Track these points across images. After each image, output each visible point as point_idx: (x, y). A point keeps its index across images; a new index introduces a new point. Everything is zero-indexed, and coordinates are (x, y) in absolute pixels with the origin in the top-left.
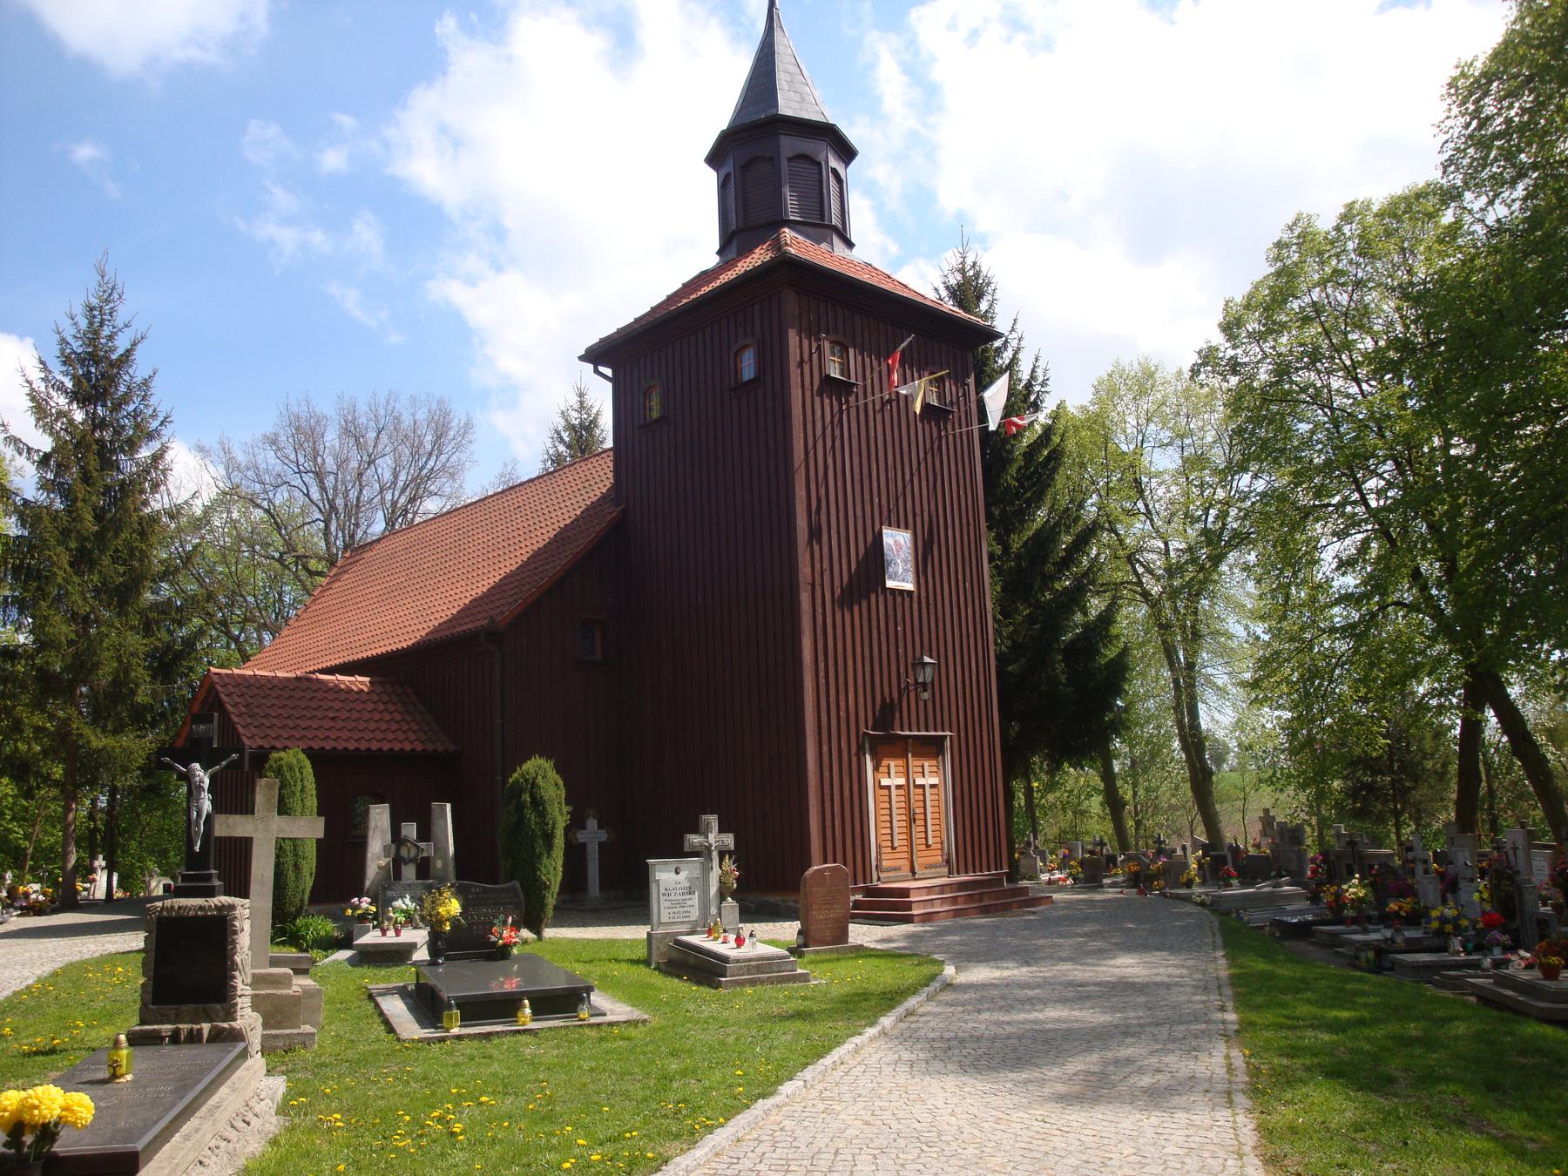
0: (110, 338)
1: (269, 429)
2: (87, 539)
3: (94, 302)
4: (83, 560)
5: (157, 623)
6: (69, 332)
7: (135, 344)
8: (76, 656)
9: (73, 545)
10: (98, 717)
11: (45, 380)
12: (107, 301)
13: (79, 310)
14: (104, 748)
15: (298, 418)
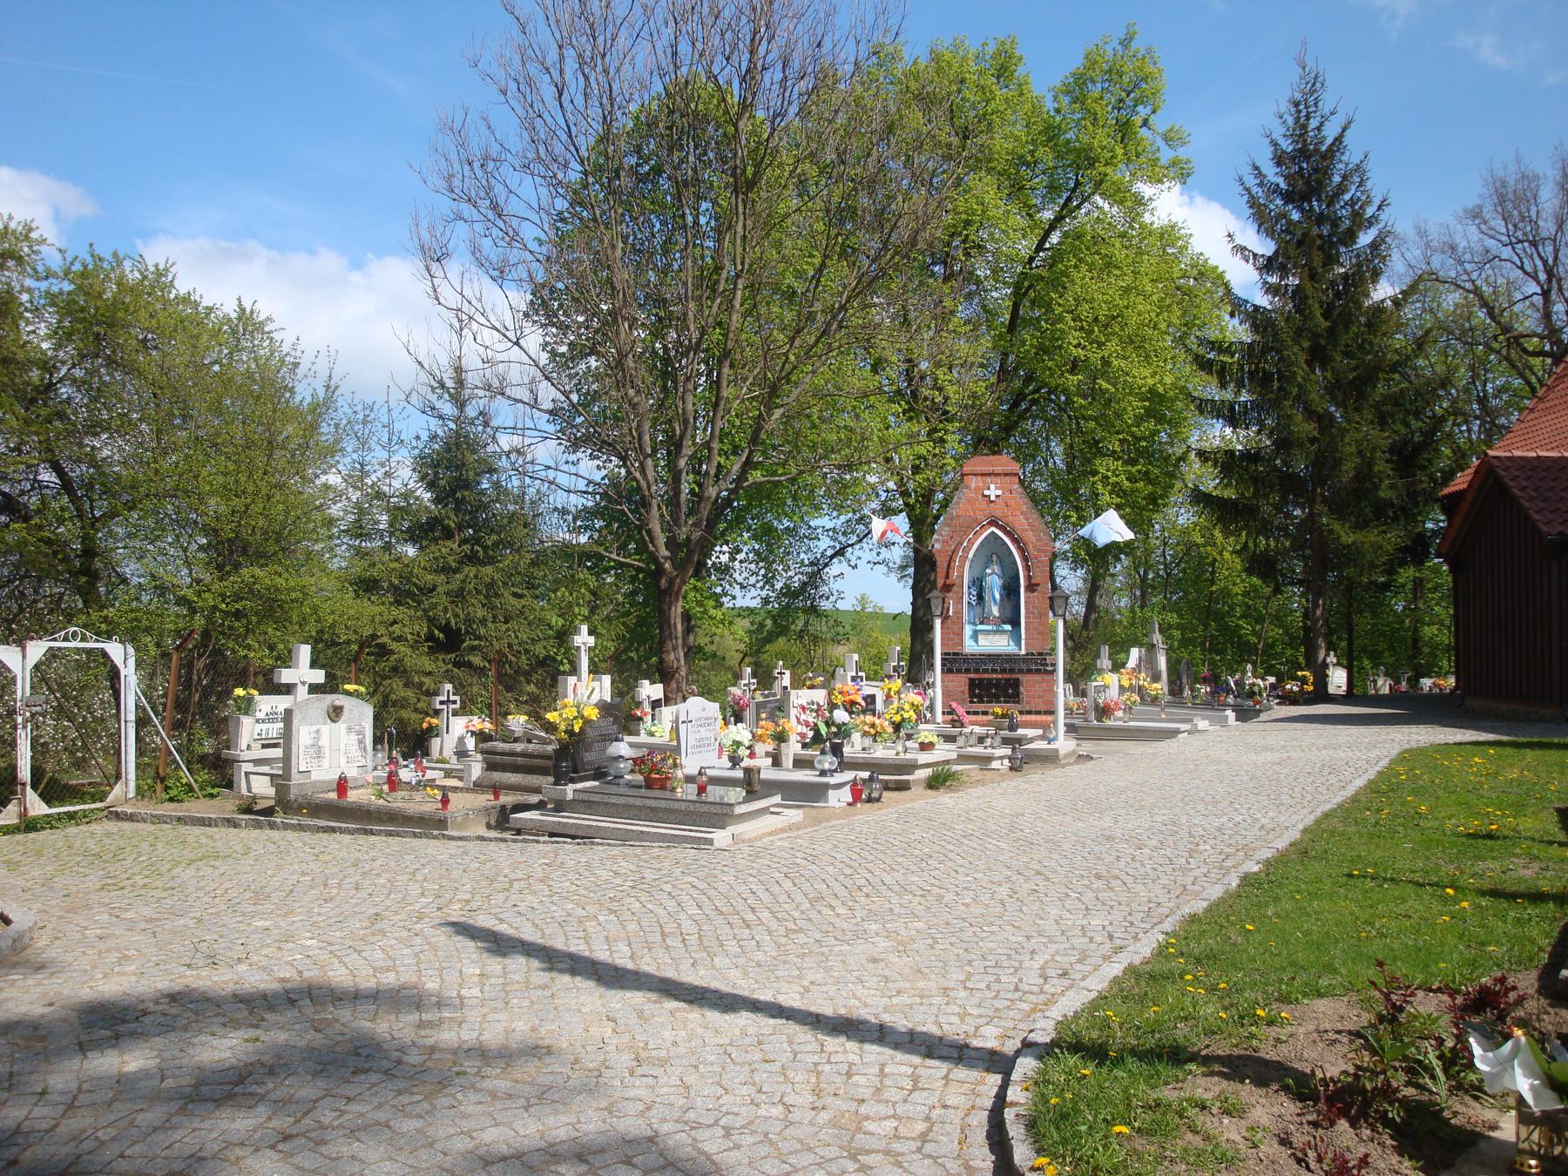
0: (1319, 129)
1: (1472, 202)
2: (1320, 336)
3: (1298, 96)
4: (1318, 356)
5: (1392, 415)
6: (1278, 132)
7: (1344, 130)
8: (1319, 453)
9: (1306, 344)
10: (1339, 511)
11: (1261, 185)
12: (1312, 92)
13: (1285, 107)
14: (1354, 543)
15: (1504, 184)
